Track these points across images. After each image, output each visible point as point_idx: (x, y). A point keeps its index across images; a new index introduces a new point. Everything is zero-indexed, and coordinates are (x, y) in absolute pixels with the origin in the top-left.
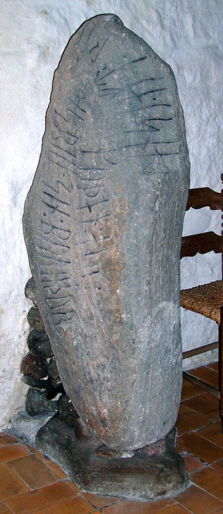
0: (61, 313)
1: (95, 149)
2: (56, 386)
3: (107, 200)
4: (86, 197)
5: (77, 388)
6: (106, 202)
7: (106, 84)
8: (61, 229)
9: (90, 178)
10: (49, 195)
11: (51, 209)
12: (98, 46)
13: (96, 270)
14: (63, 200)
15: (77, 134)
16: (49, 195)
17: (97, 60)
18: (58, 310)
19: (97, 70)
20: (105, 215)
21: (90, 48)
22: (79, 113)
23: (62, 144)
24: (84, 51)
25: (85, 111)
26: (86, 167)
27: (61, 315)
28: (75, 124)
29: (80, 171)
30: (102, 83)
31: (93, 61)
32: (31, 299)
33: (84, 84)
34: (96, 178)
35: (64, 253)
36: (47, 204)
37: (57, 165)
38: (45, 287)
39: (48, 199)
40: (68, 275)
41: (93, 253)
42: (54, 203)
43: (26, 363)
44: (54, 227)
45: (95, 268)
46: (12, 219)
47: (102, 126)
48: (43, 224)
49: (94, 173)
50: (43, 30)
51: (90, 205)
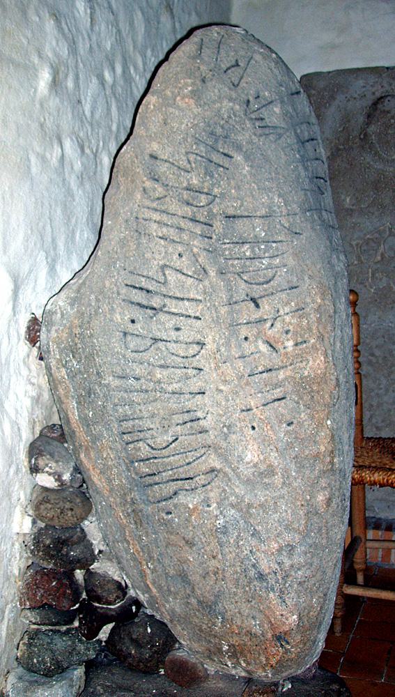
0: (181, 480)
1: (263, 212)
2: (114, 613)
3: (296, 288)
4: (243, 285)
5: (212, 598)
6: (295, 290)
7: (264, 119)
8: (176, 342)
9: (252, 256)
10: (141, 289)
11: (149, 311)
12: (237, 65)
13: (281, 395)
14: (178, 295)
15: (216, 190)
16: (141, 289)
17: (243, 84)
18: (171, 476)
19: (246, 98)
20: (293, 309)
21: (224, 67)
22: (216, 158)
23: (174, 207)
24: (216, 69)
25: (231, 157)
26: (240, 239)
27: (180, 482)
28: (208, 173)
29: (224, 247)
30: (258, 117)
31: (234, 85)
32: (50, 474)
33: (225, 116)
34: (267, 255)
35: (187, 379)
36: (139, 304)
37: (162, 242)
38: (127, 444)
39: (139, 297)
40: (200, 414)
41: (270, 370)
42: (156, 302)
43: (37, 588)
44: (155, 340)
45: (278, 393)
46: (9, 343)
47: (272, 179)
48: (129, 338)
49: (263, 247)
50: (54, 43)
51: (256, 296)
